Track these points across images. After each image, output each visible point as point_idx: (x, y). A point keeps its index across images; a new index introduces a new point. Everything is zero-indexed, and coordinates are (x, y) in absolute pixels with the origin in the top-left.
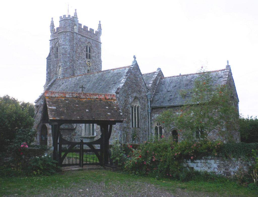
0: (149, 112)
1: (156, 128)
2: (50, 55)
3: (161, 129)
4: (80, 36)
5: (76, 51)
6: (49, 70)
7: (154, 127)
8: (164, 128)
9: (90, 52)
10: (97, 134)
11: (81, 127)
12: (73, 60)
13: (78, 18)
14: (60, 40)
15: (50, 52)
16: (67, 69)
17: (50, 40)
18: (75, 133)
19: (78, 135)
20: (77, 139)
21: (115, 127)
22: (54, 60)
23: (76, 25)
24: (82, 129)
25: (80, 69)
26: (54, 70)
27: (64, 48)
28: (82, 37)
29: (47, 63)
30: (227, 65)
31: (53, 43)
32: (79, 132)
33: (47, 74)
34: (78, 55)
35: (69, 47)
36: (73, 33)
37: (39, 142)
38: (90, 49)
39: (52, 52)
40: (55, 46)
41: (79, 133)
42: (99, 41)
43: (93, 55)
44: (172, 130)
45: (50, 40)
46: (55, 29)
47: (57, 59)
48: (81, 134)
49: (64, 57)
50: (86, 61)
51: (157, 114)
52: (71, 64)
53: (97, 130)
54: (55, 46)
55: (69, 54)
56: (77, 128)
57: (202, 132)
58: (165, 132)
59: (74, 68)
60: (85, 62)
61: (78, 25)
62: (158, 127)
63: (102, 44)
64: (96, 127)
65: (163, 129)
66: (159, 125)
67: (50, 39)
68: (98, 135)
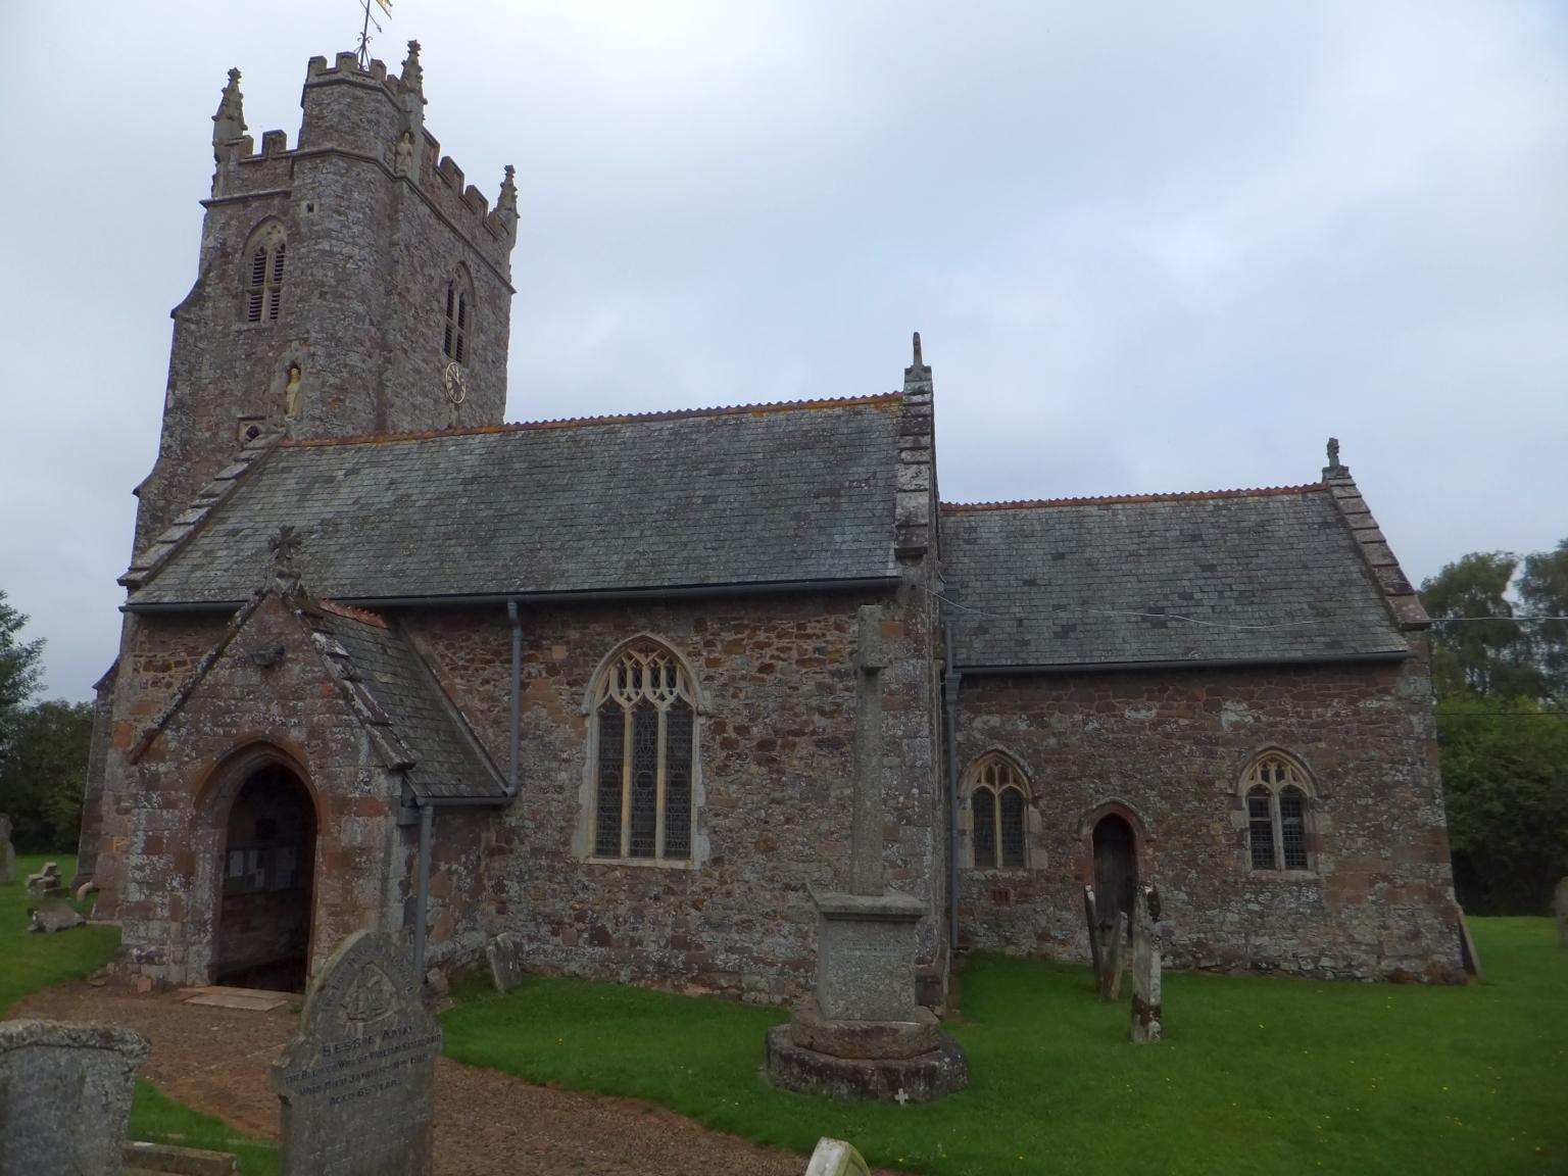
0: (948, 697)
1: (982, 801)
2: (197, 296)
3: (1014, 805)
4: (428, 211)
5: (405, 293)
6: (184, 389)
7: (968, 789)
8: (1042, 803)
9: (461, 324)
10: (715, 846)
11: (560, 789)
12: (384, 346)
13: (425, 102)
14: (304, 204)
15: (205, 271)
16: (341, 389)
17: (205, 204)
18: (508, 836)
19: (536, 852)
20: (521, 880)
21: (891, 802)
22: (234, 327)
23: (412, 136)
24: (572, 812)
25: (414, 406)
26: (223, 393)
27: (331, 254)
28: (433, 221)
29: (175, 340)
30: (1327, 463)
31: (233, 222)
32: (539, 827)
33: (167, 412)
34: (411, 322)
35: (365, 252)
36: (395, 179)
37: (208, 915)
38: (462, 304)
39: (222, 277)
40: (245, 245)
41: (547, 839)
42: (505, 277)
43: (474, 342)
44: (1097, 817)
45: (205, 204)
46: (250, 141)
47: (253, 325)
48: (566, 843)
49: (331, 310)
50: (444, 367)
51: (990, 713)
52: (370, 363)
53: (717, 815)
54: (245, 245)
55: (363, 302)
56: (525, 794)
57: (1294, 835)
58: (1050, 826)
59: (389, 392)
60: (439, 371)
61: (420, 140)
62: (996, 791)
63: (513, 296)
64: (708, 793)
65: (1036, 806)
66: (1004, 779)
67: (208, 196)
68: (727, 855)
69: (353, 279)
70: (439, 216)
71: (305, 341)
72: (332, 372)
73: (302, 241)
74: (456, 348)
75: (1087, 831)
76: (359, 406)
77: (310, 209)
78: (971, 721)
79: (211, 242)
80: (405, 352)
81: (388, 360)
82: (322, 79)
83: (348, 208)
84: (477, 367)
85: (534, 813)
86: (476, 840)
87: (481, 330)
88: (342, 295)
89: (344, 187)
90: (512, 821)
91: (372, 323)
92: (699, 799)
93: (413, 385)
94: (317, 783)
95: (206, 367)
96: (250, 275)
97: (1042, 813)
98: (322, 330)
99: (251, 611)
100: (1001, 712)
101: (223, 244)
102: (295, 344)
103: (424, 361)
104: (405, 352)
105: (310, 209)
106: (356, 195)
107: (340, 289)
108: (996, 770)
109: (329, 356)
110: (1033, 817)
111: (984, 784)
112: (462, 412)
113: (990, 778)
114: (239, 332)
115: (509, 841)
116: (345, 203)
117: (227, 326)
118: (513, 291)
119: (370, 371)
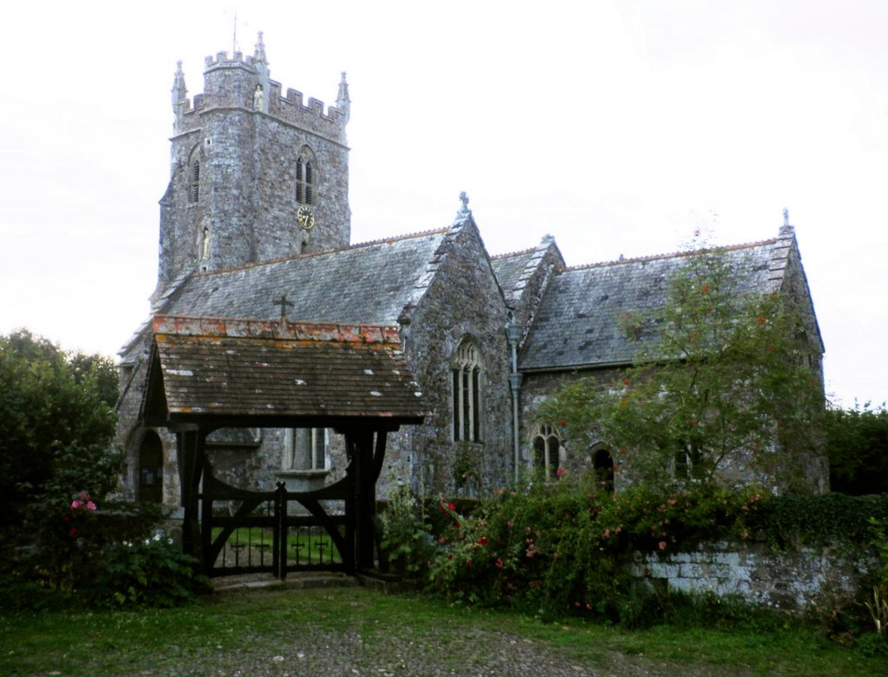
1: (539, 443)
3: (554, 445)
4: (277, 124)
6: (167, 243)
8: (567, 444)
9: (309, 179)
10: (333, 463)
11: (277, 439)
12: (252, 209)
14: (206, 140)
16: (229, 238)
17: (172, 140)
18: (260, 460)
19: (270, 467)
20: (264, 480)
22: (187, 207)
23: (261, 86)
24: (282, 448)
25: (275, 238)
26: (184, 243)
35: (237, 162)
37: (133, 491)
41: (272, 462)
44: (593, 450)
45: (172, 140)
47: (195, 204)
48: (280, 463)
50: (296, 210)
56: (265, 442)
58: (570, 456)
59: (256, 234)
60: (292, 213)
61: (267, 86)
62: (545, 438)
63: (350, 153)
65: (563, 446)
66: (550, 432)
69: (231, 177)
70: (285, 125)
71: (209, 216)
72: (223, 230)
73: (206, 161)
74: (305, 196)
75: (589, 459)
76: (238, 245)
77: (209, 142)
78: (532, 399)
79: (175, 161)
80: (266, 209)
81: (255, 217)
82: (213, 67)
83: (226, 138)
84: (323, 203)
85: (268, 450)
86: (244, 463)
87: (323, 180)
88: (226, 187)
89: (224, 127)
90: (260, 454)
91: (244, 198)
92: (327, 442)
93: (273, 226)
94: (231, 440)
95: (176, 229)
96: (193, 176)
97: (566, 450)
98: (217, 207)
99: (137, 369)
100: (547, 393)
101: (180, 161)
102: (206, 217)
103: (280, 210)
104: (266, 209)
105: (209, 142)
106: (230, 131)
107: (225, 184)
108: (546, 426)
109: (222, 221)
110: (562, 451)
111: (539, 434)
112: (313, 233)
113: (543, 431)
114: (189, 209)
115: (260, 463)
116: (225, 136)
117: (184, 205)
118: (348, 149)
119: (245, 225)
